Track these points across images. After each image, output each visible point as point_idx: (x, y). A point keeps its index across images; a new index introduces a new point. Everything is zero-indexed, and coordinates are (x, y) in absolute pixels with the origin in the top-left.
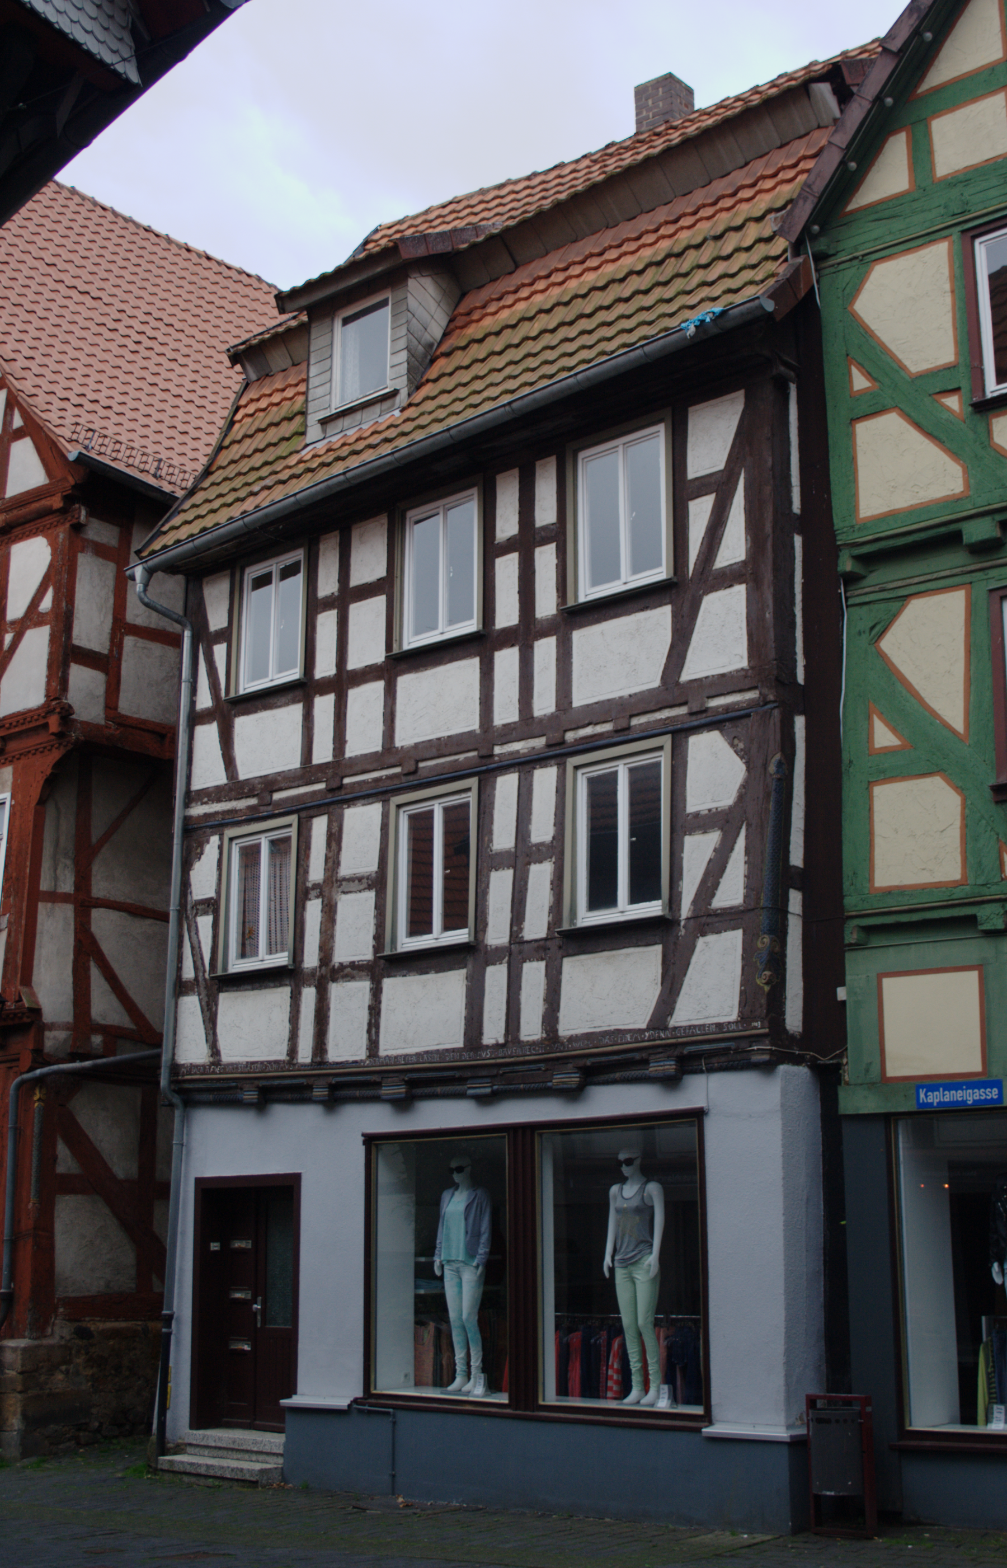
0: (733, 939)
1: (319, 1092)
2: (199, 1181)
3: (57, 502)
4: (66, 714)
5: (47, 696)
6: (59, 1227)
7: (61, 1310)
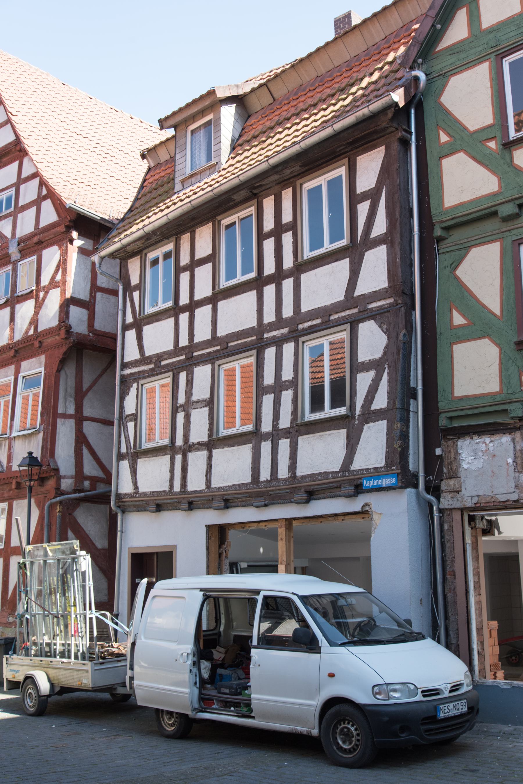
5: (59, 321)
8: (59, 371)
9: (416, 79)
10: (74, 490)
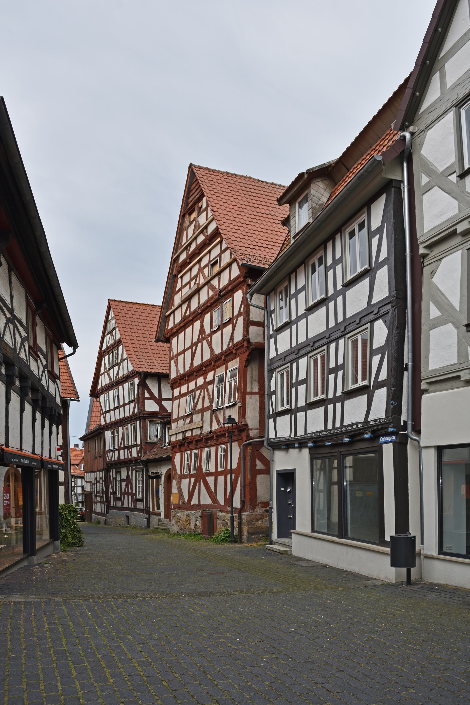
0: (384, 390)
1: (296, 445)
2: (276, 471)
3: (242, 279)
4: (248, 341)
5: (243, 336)
6: (258, 483)
7: (260, 505)
8: (246, 366)
9: (404, 137)
10: (259, 436)
